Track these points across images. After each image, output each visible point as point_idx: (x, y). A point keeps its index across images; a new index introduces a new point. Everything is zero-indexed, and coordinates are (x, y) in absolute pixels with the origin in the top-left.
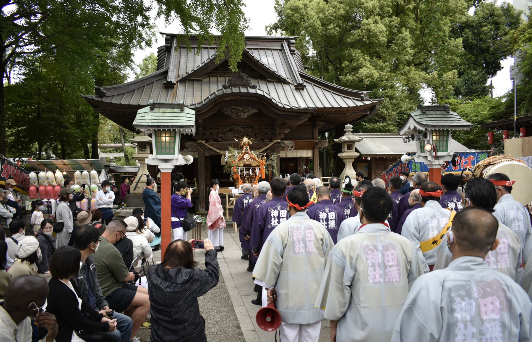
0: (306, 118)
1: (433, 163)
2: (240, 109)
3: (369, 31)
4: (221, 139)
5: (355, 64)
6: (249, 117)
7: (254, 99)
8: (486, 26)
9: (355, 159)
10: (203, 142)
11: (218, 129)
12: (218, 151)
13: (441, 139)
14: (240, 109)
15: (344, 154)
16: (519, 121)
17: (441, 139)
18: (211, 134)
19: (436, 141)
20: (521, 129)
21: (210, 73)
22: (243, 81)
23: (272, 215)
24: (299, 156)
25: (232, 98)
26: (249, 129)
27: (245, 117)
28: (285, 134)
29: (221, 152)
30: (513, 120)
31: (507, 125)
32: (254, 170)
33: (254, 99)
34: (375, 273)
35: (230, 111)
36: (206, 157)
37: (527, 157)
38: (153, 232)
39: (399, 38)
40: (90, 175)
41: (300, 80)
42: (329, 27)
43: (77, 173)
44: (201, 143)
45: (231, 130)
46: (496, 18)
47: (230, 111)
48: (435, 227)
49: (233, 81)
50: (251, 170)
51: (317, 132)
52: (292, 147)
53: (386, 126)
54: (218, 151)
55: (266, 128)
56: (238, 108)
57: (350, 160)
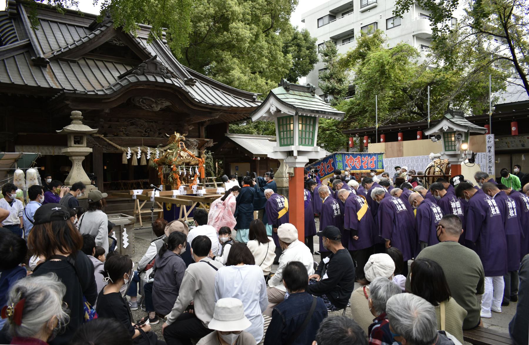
0: (217, 115)
2: (153, 100)
3: (237, 35)
5: (225, 66)
6: (162, 110)
7: (170, 90)
8: (291, 46)
9: (86, 157)
10: (102, 136)
12: (119, 147)
14: (153, 100)
15: (69, 150)
16: (380, 129)
18: (110, 127)
19: (302, 131)
20: (382, 136)
21: (86, 54)
22: (156, 69)
23: (452, 207)
24: (56, 154)
25: (145, 87)
27: (159, 109)
29: (123, 149)
30: (375, 128)
31: (367, 132)
32: (194, 169)
33: (170, 90)
35: (142, 102)
36: (104, 154)
37: (390, 159)
39: (257, 46)
40: (25, 174)
41: (190, 77)
42: (198, 24)
43: (19, 172)
44: (99, 137)
45: (132, 124)
46: (299, 41)
47: (142, 102)
49: (146, 68)
50: (190, 169)
51: (204, 130)
53: (249, 128)
54: (119, 147)
56: (151, 99)
57: (80, 158)
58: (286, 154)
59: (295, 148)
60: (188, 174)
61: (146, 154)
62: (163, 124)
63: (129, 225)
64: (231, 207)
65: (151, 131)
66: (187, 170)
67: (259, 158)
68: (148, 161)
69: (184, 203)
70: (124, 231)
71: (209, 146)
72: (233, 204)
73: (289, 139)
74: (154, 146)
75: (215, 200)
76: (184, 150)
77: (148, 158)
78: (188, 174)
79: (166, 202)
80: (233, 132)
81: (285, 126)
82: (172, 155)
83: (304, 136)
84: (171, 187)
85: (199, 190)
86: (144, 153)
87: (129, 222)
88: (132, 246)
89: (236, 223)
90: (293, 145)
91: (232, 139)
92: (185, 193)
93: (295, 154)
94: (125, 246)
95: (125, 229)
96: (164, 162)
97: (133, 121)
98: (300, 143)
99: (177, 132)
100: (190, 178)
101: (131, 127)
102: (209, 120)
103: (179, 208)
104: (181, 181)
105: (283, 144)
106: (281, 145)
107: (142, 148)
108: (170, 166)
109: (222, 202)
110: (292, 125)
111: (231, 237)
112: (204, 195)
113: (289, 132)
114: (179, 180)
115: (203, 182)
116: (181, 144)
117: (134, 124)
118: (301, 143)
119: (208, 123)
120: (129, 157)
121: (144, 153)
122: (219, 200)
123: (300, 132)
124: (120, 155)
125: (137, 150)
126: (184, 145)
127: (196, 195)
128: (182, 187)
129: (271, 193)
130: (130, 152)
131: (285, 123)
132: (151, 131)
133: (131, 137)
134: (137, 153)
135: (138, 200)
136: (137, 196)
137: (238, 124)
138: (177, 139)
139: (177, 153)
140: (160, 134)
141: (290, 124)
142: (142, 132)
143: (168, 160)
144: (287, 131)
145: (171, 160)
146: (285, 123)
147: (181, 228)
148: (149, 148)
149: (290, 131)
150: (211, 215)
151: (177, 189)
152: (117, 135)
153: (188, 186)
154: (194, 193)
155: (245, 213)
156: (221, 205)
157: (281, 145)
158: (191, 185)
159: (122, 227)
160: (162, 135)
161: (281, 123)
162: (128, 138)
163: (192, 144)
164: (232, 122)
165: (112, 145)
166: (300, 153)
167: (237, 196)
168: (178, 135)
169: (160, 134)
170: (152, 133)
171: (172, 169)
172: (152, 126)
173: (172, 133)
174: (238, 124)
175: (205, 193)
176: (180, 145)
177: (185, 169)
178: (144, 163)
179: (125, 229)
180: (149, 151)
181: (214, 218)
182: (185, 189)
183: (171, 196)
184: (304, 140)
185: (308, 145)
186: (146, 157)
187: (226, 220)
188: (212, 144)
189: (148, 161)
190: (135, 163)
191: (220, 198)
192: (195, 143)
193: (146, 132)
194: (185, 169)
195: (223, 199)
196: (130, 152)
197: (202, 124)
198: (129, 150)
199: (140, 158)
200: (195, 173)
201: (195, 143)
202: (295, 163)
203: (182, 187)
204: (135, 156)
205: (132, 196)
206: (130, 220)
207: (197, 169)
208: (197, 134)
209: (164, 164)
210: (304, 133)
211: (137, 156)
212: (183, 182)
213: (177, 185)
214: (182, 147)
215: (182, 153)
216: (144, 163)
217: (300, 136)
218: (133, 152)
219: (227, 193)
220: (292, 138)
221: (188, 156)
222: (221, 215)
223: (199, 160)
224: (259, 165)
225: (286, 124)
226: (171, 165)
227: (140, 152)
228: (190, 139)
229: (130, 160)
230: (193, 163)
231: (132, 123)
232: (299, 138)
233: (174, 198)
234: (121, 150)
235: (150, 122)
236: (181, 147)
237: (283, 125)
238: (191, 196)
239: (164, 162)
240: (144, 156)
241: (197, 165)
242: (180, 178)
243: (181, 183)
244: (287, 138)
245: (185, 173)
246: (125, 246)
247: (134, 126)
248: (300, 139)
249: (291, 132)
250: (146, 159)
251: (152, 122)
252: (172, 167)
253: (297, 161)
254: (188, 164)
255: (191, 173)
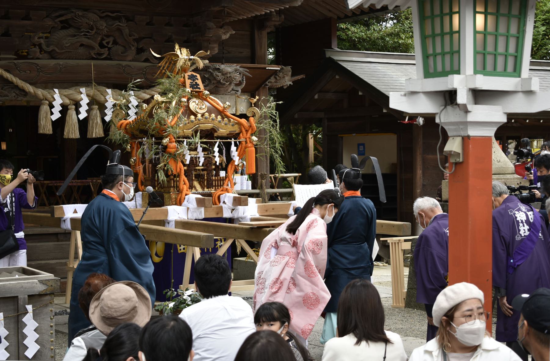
1: (471, 118)
4: (37, 49)
11: (27, 18)
12: (30, 88)
13: (502, 29)
17: (502, 29)
19: (485, 33)
26: (123, 24)
28: (222, 44)
29: (40, 92)
34: (524, 228)
38: (506, 185)
45: (66, 25)
48: (524, 221)
50: (216, 149)
52: (240, 84)
53: (398, 35)
54: (30, 88)
55: (168, 24)
58: (441, 100)
59: (461, 83)
60: (209, 161)
61: (102, 108)
62: (148, 24)
63: (41, 295)
64: (314, 252)
65: (115, 43)
66: (208, 150)
67: (421, 121)
68: (106, 126)
69: (194, 241)
70: (26, 312)
71: (279, 85)
72: (317, 243)
73: (447, 58)
74: (120, 86)
75: (270, 232)
76: (198, 95)
77: (107, 119)
78: (209, 161)
79: (152, 238)
80: (355, 45)
81: (438, 21)
82: (167, 110)
83: (490, 48)
84: (162, 197)
85: (241, 208)
86: (97, 104)
87: (41, 288)
88: (50, 354)
89: (328, 296)
90: (458, 72)
91: (344, 65)
92: (201, 213)
93: (462, 98)
94: (30, 354)
95: (29, 308)
96: (146, 130)
97: (69, 16)
98: (479, 68)
99: (181, 47)
100: (217, 174)
101: (63, 33)
102: (279, 12)
103: (184, 255)
104: (190, 180)
105: (431, 71)
106: (428, 74)
107: (92, 92)
108: (159, 138)
109: (288, 236)
110: (456, 18)
111: (291, 330)
112: (252, 220)
113: (447, 38)
114: (183, 177)
115: (261, 188)
116: (192, 77)
117: (70, 26)
118: (481, 68)
119: (277, 21)
120: (56, 115)
121: (97, 104)
122: (281, 232)
123: (480, 37)
124: (32, 111)
125: (78, 97)
126: (199, 82)
127: (231, 220)
128: (192, 198)
129: (432, 210)
130: (58, 101)
131: (437, 11)
132: (115, 43)
133: (61, 62)
134: (77, 105)
135: (78, 233)
136: (73, 220)
137: (367, 25)
138: (180, 64)
139: (179, 102)
140: (140, 51)
141: (451, 14)
142: (92, 48)
143: (154, 124)
144: (442, 34)
145: (162, 123)
146: (437, 11)
147: (127, 300)
148: (109, 91)
149: (452, 33)
150: (261, 273)
151: (180, 204)
152: (25, 57)
153: (210, 195)
154: (227, 214)
155: (347, 270)
156: (286, 247)
157: (428, 74)
158: (219, 192)
159: (21, 303)
160: (144, 56)
161: (428, 12)
162: (53, 62)
163: (230, 80)
164: (346, 17)
165: (12, 83)
166: (479, 96)
167: (330, 218)
168: (183, 54)
169: (140, 51)
170: (118, 49)
171: (165, 148)
172: (119, 30)
173: (166, 48)
174: (367, 25)
175: (257, 216)
176: (188, 82)
177: (200, 149)
178: (97, 131)
179: (29, 308)
180: (110, 98)
181: (269, 282)
182: (200, 203)
183: (163, 223)
184: (489, 60)
185: (504, 73)
186: (103, 115)
187: (301, 290)
188: (287, 81)
189: (106, 126)
190: (72, 131)
191: (284, 227)
192: (238, 78)
193: (102, 46)
194: (200, 149)
195: (292, 229)
196: (58, 101)
197: (259, 22)
198: (57, 96)
199: (86, 119)
200: (229, 159)
201: (238, 78)
202: (466, 124)
203: (192, 198)
204: (72, 112)
205: (60, 221)
206: (41, 282)
207: (233, 148)
208: (246, 52)
209: (144, 133)
210: (490, 40)
211: (78, 113)
212: (196, 184)
213: (180, 191)
214: (194, 86)
215: (193, 105)
216: (97, 131)
217: (480, 49)
218: (67, 101)
219: (302, 214)
220: (456, 53)
221: (210, 112)
222: (287, 274)
223: (240, 124)
224: (420, 141)
225: (442, 16)
226: (162, 138)
227: (85, 101)
228: (222, 67)
229: (59, 125)
230: (223, 131)
231: (66, 22)
232: (476, 53)
233: (171, 228)
234: (35, 96)
235: (114, 19)
236: (192, 86)
237: (433, 17)
238: (217, 223)
239: (146, 130)
240: (96, 111)
241: (236, 136)
242: (187, 174)
243: (191, 187)
244: (443, 54)
245: (202, 160)
246: (30, 354)
247: (71, 31)
248: (480, 58)
249: (455, 35)
250: (103, 121)
251: (118, 18)
252: (165, 141)
253: (471, 118)
254: (209, 135)
255: (217, 159)
